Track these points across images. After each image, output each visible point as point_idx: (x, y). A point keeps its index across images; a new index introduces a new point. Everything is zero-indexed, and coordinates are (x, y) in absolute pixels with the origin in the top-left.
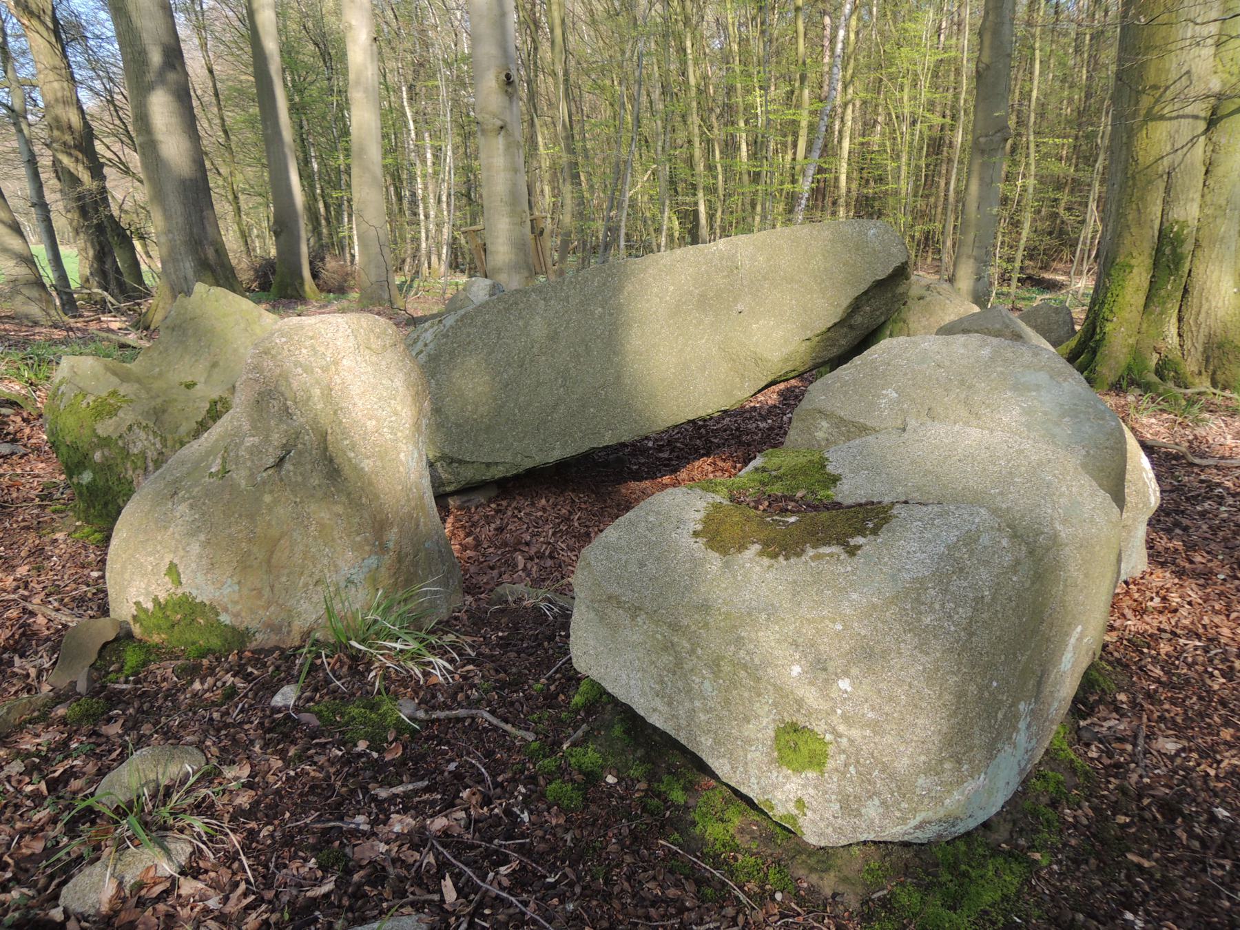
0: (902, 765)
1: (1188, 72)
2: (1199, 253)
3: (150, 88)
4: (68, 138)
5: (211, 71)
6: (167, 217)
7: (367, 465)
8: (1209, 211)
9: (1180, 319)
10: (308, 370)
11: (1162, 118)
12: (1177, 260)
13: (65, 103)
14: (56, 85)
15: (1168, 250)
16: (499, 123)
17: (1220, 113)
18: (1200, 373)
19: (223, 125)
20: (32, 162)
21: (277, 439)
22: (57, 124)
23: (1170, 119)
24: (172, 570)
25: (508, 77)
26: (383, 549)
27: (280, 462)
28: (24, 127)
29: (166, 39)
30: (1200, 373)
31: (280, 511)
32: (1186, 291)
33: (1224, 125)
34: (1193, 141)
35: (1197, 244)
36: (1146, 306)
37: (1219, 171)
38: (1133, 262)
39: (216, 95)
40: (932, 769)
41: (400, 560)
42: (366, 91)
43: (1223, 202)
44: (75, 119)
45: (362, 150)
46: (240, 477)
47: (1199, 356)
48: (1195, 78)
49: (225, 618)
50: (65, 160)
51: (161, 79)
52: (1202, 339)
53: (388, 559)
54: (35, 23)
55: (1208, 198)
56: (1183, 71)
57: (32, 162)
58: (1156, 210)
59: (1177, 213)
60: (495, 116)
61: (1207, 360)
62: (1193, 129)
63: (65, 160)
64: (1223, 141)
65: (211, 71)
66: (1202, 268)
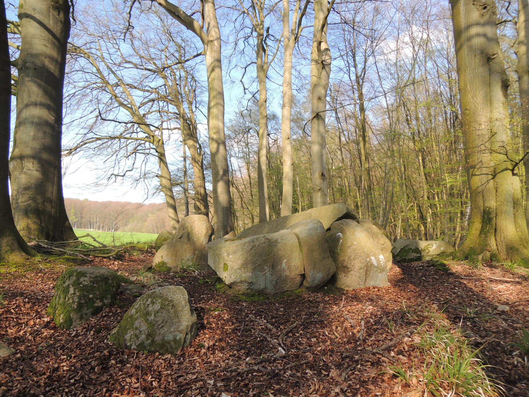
0: (235, 267)
1: (481, 161)
2: (497, 217)
3: (218, 181)
4: (200, 197)
5: (249, 176)
6: (218, 218)
7: (195, 240)
8: (498, 203)
9: (496, 240)
10: (189, 223)
11: (476, 175)
12: (490, 220)
13: (200, 186)
14: (199, 182)
15: (486, 217)
16: (319, 188)
17: (496, 172)
18: (507, 259)
19: (251, 193)
20: (187, 204)
21: (181, 233)
22: (197, 193)
23: (478, 175)
24: (162, 256)
25: (322, 174)
26: (195, 254)
27: (181, 238)
28: (187, 193)
29: (225, 167)
30: (507, 259)
31: (179, 246)
32: (496, 230)
33: (498, 176)
34: (488, 181)
35: (496, 215)
36: (480, 235)
37: (499, 190)
38: (475, 220)
39: (250, 183)
40: (240, 269)
41: (198, 257)
42: (288, 180)
43: (502, 200)
44: (202, 191)
45: (286, 199)
46: (174, 240)
47: (505, 253)
48: (483, 163)
49: (168, 265)
50: (198, 203)
51: (222, 179)
52: (504, 247)
53: (195, 257)
54: (196, 164)
55: (498, 199)
56: (480, 160)
57: (187, 204)
58: (481, 203)
59: (487, 204)
60: (318, 186)
61: (508, 254)
62: (487, 178)
63: (198, 203)
64: (499, 181)
65: (249, 176)
66: (499, 223)
